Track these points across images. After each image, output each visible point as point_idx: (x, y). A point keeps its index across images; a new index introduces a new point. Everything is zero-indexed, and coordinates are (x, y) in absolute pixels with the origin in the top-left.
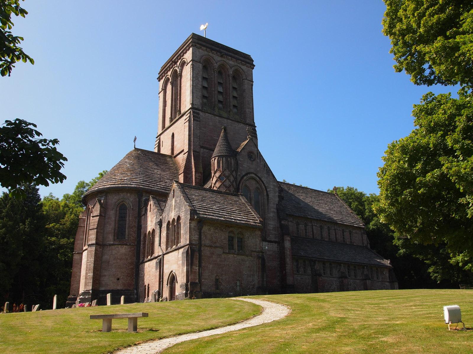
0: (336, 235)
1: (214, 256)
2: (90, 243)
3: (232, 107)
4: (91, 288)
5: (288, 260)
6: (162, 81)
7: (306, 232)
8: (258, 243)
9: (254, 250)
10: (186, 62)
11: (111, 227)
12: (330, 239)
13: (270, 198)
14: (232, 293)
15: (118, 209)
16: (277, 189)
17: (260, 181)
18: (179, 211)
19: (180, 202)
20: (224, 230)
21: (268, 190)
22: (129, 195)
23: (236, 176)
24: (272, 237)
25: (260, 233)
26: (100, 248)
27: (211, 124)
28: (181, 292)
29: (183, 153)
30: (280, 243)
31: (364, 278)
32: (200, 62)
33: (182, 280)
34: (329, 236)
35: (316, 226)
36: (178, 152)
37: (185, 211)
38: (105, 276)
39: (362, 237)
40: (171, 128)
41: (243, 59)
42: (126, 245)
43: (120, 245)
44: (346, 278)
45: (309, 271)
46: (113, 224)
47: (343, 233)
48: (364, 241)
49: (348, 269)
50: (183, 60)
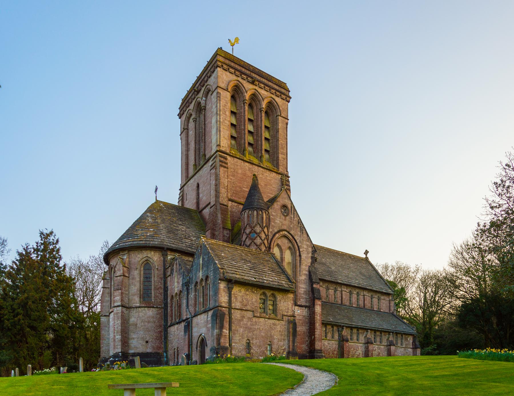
0: (364, 301)
1: (244, 320)
2: (116, 304)
3: (263, 152)
4: (120, 350)
5: (318, 325)
6: (184, 117)
7: (335, 298)
8: (290, 306)
9: (286, 314)
10: (211, 90)
11: (136, 288)
12: (358, 305)
13: (302, 260)
14: (262, 358)
15: (142, 269)
16: (310, 250)
17: (293, 240)
18: (208, 271)
19: (208, 260)
20: (255, 292)
21: (301, 250)
22: (152, 253)
23: (268, 232)
24: (302, 301)
25: (292, 296)
26: (126, 310)
27: (240, 171)
28: (211, 356)
29: (209, 207)
30: (311, 307)
31: (388, 344)
32: (227, 90)
33: (212, 343)
34: (358, 302)
35: (345, 291)
36: (204, 206)
37: (214, 270)
38: (134, 338)
39: (390, 304)
40: (195, 177)
41: (278, 89)
42: (153, 307)
43: (146, 307)
44: (372, 343)
45: (336, 337)
46: (138, 285)
47: (372, 299)
48: (391, 307)
49: (375, 335)
50: (208, 87)
